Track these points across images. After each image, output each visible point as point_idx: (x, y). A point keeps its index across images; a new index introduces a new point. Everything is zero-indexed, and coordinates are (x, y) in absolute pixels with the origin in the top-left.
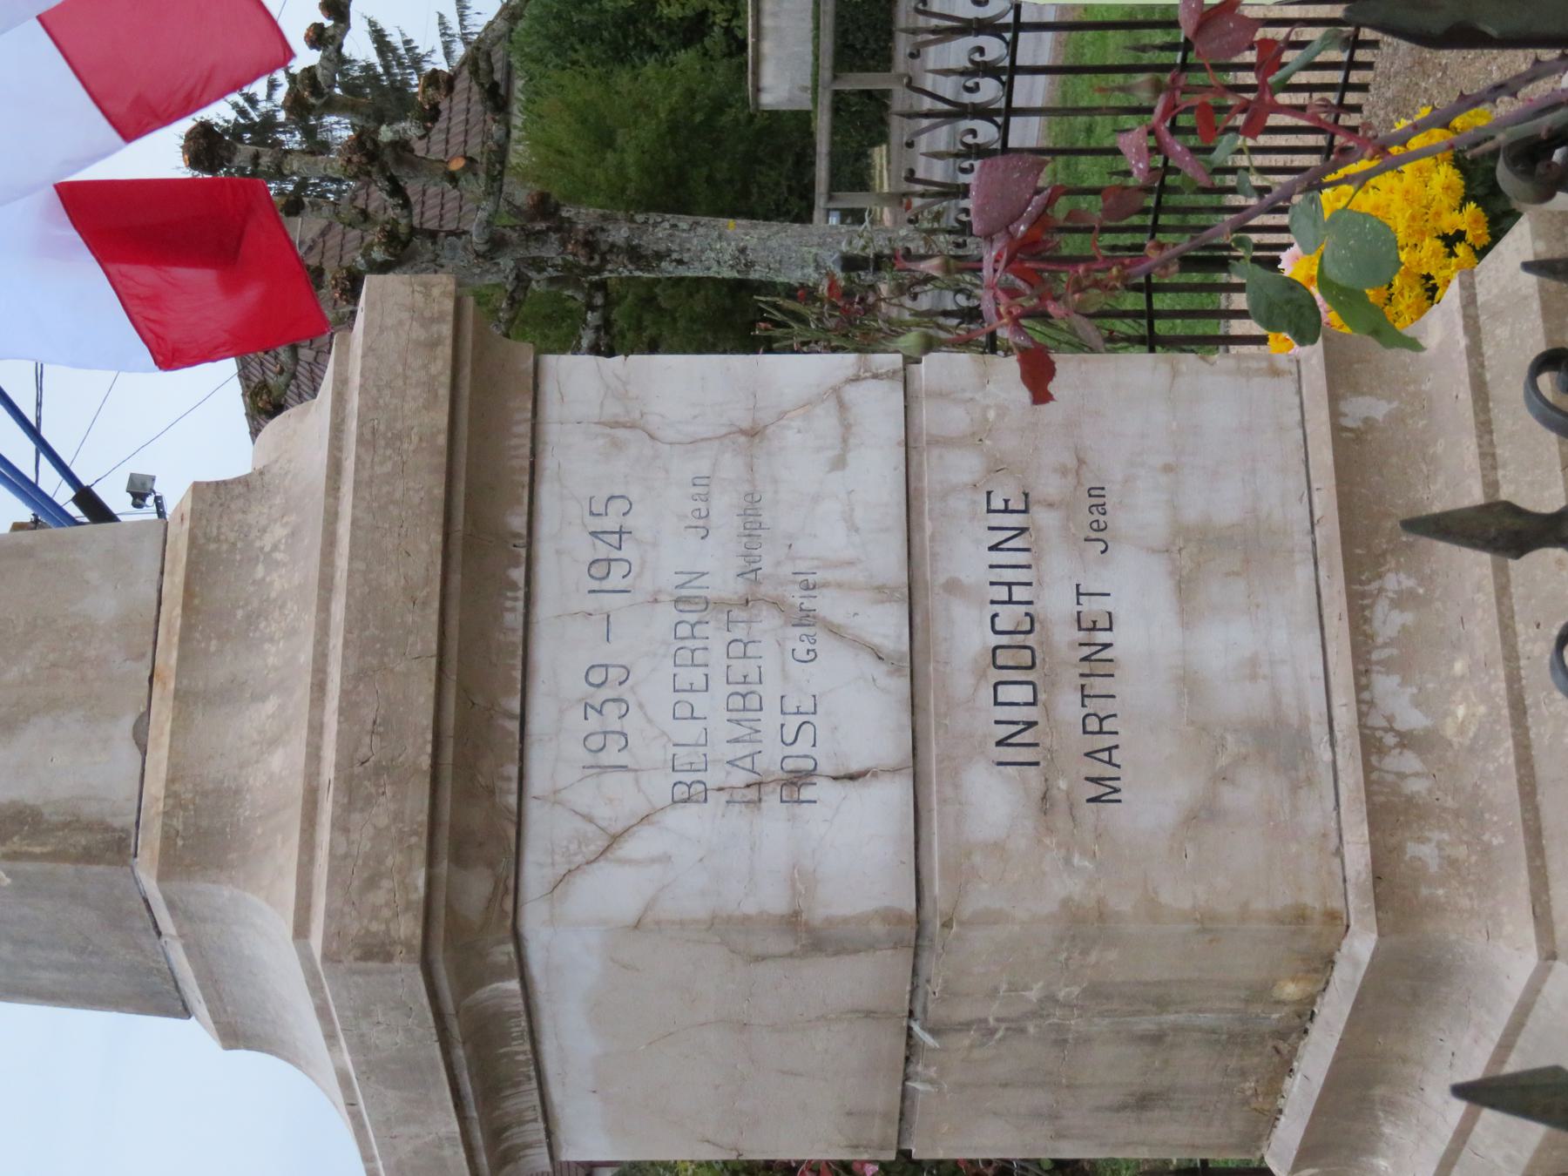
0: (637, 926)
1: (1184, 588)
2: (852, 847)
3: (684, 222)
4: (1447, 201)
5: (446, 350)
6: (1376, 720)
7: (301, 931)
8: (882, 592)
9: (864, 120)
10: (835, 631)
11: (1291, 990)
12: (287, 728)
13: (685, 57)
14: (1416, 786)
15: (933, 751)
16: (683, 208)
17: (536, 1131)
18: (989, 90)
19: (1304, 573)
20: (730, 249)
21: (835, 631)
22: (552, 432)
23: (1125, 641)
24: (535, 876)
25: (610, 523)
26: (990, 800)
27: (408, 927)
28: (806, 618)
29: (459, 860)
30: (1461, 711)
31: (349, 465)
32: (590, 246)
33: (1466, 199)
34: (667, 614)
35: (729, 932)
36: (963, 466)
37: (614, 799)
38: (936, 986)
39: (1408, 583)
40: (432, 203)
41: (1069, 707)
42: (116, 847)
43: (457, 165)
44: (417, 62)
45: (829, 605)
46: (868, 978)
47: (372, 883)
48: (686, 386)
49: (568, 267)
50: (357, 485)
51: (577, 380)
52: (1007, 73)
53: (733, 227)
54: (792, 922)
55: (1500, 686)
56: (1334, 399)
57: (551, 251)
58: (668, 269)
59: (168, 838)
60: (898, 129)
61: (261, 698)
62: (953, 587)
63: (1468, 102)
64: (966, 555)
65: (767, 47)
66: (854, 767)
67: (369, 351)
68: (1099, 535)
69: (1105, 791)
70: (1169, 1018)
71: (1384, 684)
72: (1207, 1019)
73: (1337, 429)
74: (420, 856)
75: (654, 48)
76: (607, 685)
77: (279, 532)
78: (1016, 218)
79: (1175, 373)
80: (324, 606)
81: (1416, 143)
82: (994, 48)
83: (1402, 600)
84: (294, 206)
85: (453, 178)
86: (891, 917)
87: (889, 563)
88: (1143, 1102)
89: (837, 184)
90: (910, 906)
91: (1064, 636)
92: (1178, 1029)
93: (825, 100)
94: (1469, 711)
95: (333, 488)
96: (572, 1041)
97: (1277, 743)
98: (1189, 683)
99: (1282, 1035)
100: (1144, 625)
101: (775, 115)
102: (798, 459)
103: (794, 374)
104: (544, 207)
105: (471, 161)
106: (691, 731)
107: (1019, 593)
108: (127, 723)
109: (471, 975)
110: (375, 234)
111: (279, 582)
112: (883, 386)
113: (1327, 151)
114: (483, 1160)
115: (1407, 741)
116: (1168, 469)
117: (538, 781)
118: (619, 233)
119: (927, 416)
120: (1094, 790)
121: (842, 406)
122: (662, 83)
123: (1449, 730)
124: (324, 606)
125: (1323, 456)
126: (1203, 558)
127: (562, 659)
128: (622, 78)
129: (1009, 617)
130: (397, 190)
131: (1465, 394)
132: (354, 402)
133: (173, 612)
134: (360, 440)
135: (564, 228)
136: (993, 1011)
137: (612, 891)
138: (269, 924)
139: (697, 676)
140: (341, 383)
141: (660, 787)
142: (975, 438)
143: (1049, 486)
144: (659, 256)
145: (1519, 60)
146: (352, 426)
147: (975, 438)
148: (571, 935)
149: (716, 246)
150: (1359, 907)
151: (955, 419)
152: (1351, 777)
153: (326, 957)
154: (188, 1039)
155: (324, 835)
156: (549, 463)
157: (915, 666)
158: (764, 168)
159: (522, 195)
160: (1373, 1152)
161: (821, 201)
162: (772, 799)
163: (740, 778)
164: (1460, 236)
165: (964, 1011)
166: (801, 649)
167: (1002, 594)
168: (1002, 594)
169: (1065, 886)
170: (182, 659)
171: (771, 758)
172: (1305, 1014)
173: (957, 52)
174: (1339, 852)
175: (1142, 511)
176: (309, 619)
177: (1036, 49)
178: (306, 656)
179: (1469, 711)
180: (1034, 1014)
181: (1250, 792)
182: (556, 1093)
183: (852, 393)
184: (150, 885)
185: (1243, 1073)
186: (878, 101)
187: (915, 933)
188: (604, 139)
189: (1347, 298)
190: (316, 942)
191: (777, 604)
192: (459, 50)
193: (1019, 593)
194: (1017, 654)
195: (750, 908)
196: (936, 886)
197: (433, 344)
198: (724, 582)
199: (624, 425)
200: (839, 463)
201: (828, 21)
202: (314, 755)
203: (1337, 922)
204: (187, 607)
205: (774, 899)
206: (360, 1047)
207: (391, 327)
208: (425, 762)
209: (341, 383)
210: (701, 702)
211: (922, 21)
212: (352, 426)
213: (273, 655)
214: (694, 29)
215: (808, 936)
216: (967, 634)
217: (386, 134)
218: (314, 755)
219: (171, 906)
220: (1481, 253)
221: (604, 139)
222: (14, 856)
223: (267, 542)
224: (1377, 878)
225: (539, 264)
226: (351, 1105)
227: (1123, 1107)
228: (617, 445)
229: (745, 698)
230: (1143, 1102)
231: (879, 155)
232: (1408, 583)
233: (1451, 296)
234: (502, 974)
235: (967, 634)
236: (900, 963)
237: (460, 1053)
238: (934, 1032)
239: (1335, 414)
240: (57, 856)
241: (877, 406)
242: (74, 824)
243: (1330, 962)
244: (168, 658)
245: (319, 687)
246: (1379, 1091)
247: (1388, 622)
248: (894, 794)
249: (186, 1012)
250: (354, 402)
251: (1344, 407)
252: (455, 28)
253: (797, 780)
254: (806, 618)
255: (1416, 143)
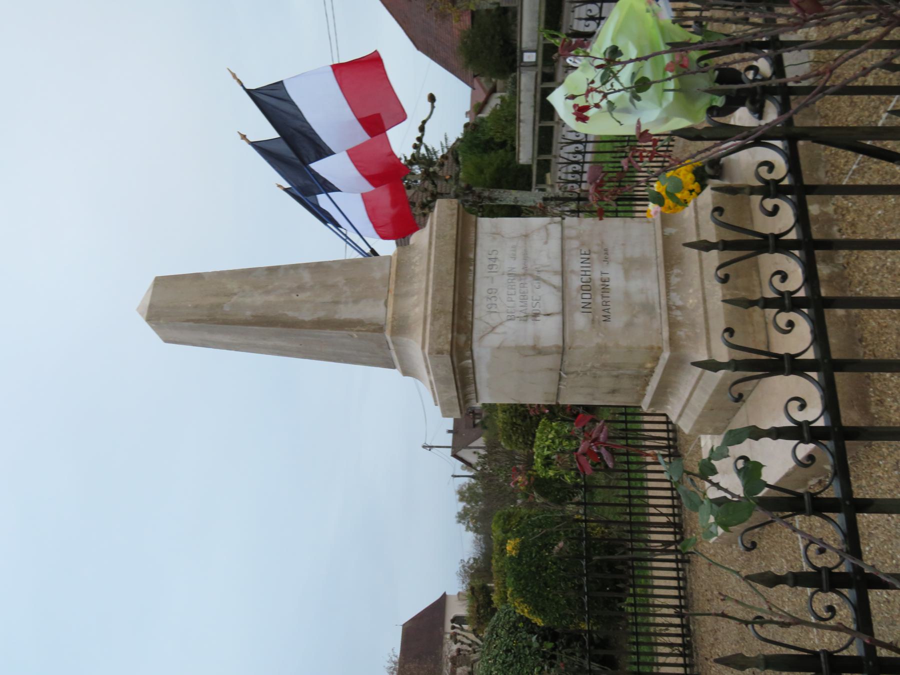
0: (498, 348)
1: (627, 272)
2: (548, 331)
3: (502, 191)
4: (691, 182)
5: (456, 216)
6: (671, 303)
7: (423, 348)
8: (556, 273)
9: (545, 167)
10: (544, 281)
11: (649, 365)
12: (420, 302)
13: (501, 151)
14: (680, 318)
15: (567, 309)
16: (501, 188)
17: (473, 396)
18: (579, 157)
19: (654, 269)
20: (513, 197)
21: (544, 281)
22: (480, 235)
23: (612, 284)
24: (476, 336)
25: (493, 256)
26: (580, 321)
27: (447, 347)
28: (538, 279)
29: (458, 332)
30: (691, 301)
31: (434, 243)
32: (479, 197)
33: (696, 181)
34: (506, 277)
35: (520, 350)
36: (575, 244)
37: (494, 319)
38: (566, 363)
39: (679, 271)
40: (442, 186)
41: (599, 299)
42: (380, 329)
43: (447, 177)
44: (435, 153)
45: (544, 276)
46: (551, 361)
47: (439, 337)
48: (509, 224)
49: (474, 202)
50: (436, 247)
51: (486, 224)
52: (584, 153)
53: (514, 192)
54: (534, 348)
55: (700, 295)
56: (663, 228)
57: (470, 198)
58: (498, 202)
59: (392, 327)
60: (553, 167)
61: (413, 296)
62: (572, 272)
63: (699, 152)
64: (575, 264)
65: (521, 149)
66: (549, 312)
67: (438, 217)
68: (606, 260)
69: (607, 319)
70: (621, 371)
71: (673, 295)
72: (629, 372)
73: (663, 235)
74: (450, 331)
75: (493, 149)
76: (492, 293)
77: (417, 258)
78: (597, 179)
79: (625, 222)
80: (428, 274)
81: (687, 162)
82: (581, 147)
83: (678, 276)
84: (409, 187)
85: (446, 180)
86: (557, 346)
87: (557, 266)
88: (614, 392)
89: (538, 182)
90: (561, 344)
91: (598, 283)
92: (622, 374)
93: (535, 162)
94: (693, 301)
95: (430, 248)
96: (483, 375)
97: (647, 308)
98: (627, 295)
99: (646, 376)
100: (617, 281)
101: (523, 166)
102: (536, 242)
103: (536, 222)
104: (469, 187)
105: (451, 176)
106: (511, 304)
107: (588, 273)
108: (383, 301)
109: (461, 358)
110: (429, 194)
111: (417, 270)
112: (556, 225)
113: (662, 167)
114: (462, 402)
115: (678, 308)
116: (623, 245)
117: (476, 315)
118: (486, 194)
119: (566, 232)
120: (605, 318)
121: (547, 230)
122: (496, 158)
123: (688, 306)
124: (428, 274)
125: (660, 242)
126: (631, 265)
127: (482, 287)
128: (486, 157)
129: (585, 278)
130: (433, 183)
131: (694, 227)
132: (435, 228)
133: (393, 276)
134: (437, 237)
135: (473, 192)
136: (579, 369)
137: (493, 340)
138: (416, 348)
139: (512, 291)
140: (432, 224)
141: (504, 316)
142: (577, 237)
143: (595, 248)
144: (496, 199)
145: (708, 144)
146: (434, 234)
147: (577, 237)
148: (483, 350)
149: (510, 197)
150: (666, 346)
151: (573, 233)
152: (665, 316)
153: (429, 354)
154: (394, 374)
155: (428, 326)
156: (479, 242)
157: (563, 290)
158: (520, 178)
159: (463, 185)
160: (667, 404)
161: (534, 186)
162: (530, 320)
163: (523, 315)
164: (693, 190)
165: (572, 369)
166: (537, 285)
167: (583, 273)
168: (583, 273)
169: (597, 340)
170: (396, 287)
171: (530, 310)
172: (652, 371)
173: (572, 148)
174: (661, 333)
175: (617, 254)
176: (424, 278)
177: (590, 147)
178: (424, 286)
179: (693, 301)
180: (590, 370)
181: (641, 319)
182: (479, 387)
183: (550, 227)
184: (388, 337)
185: (637, 385)
186: (548, 162)
187: (562, 351)
188: (481, 172)
189: (671, 195)
190: (426, 350)
191: (531, 275)
192: (446, 150)
193: (588, 273)
194: (587, 287)
195: (524, 344)
196: (567, 340)
197: (453, 215)
198: (519, 270)
199: (496, 234)
200: (546, 243)
201: (536, 142)
202: (426, 308)
203: (660, 349)
204: (397, 275)
205: (530, 342)
206: (435, 375)
207: (444, 210)
208: (451, 310)
209: (432, 224)
210: (514, 298)
211: (563, 141)
212: (434, 234)
213: (416, 286)
214: (503, 145)
215: (538, 351)
216: (575, 282)
217: (431, 170)
218: (426, 308)
219: (393, 342)
220: (698, 194)
221: (481, 172)
222: (358, 331)
223: (414, 260)
224: (670, 339)
225: (467, 201)
226: (432, 389)
227: (609, 393)
228: (494, 238)
229: (524, 297)
230: (614, 392)
231: (548, 175)
232: (679, 271)
233: (691, 204)
234: (468, 358)
235: (575, 282)
236: (558, 357)
237: (458, 376)
238: (566, 374)
239: (663, 232)
240: (366, 331)
241: (555, 230)
242: (371, 324)
243: (658, 359)
244: (392, 287)
245: (427, 293)
246: (669, 390)
247: (674, 280)
248: (558, 319)
249: (394, 368)
250: (435, 228)
251: (665, 230)
252: (444, 145)
253: (536, 315)
254: (538, 279)
255: (687, 162)
